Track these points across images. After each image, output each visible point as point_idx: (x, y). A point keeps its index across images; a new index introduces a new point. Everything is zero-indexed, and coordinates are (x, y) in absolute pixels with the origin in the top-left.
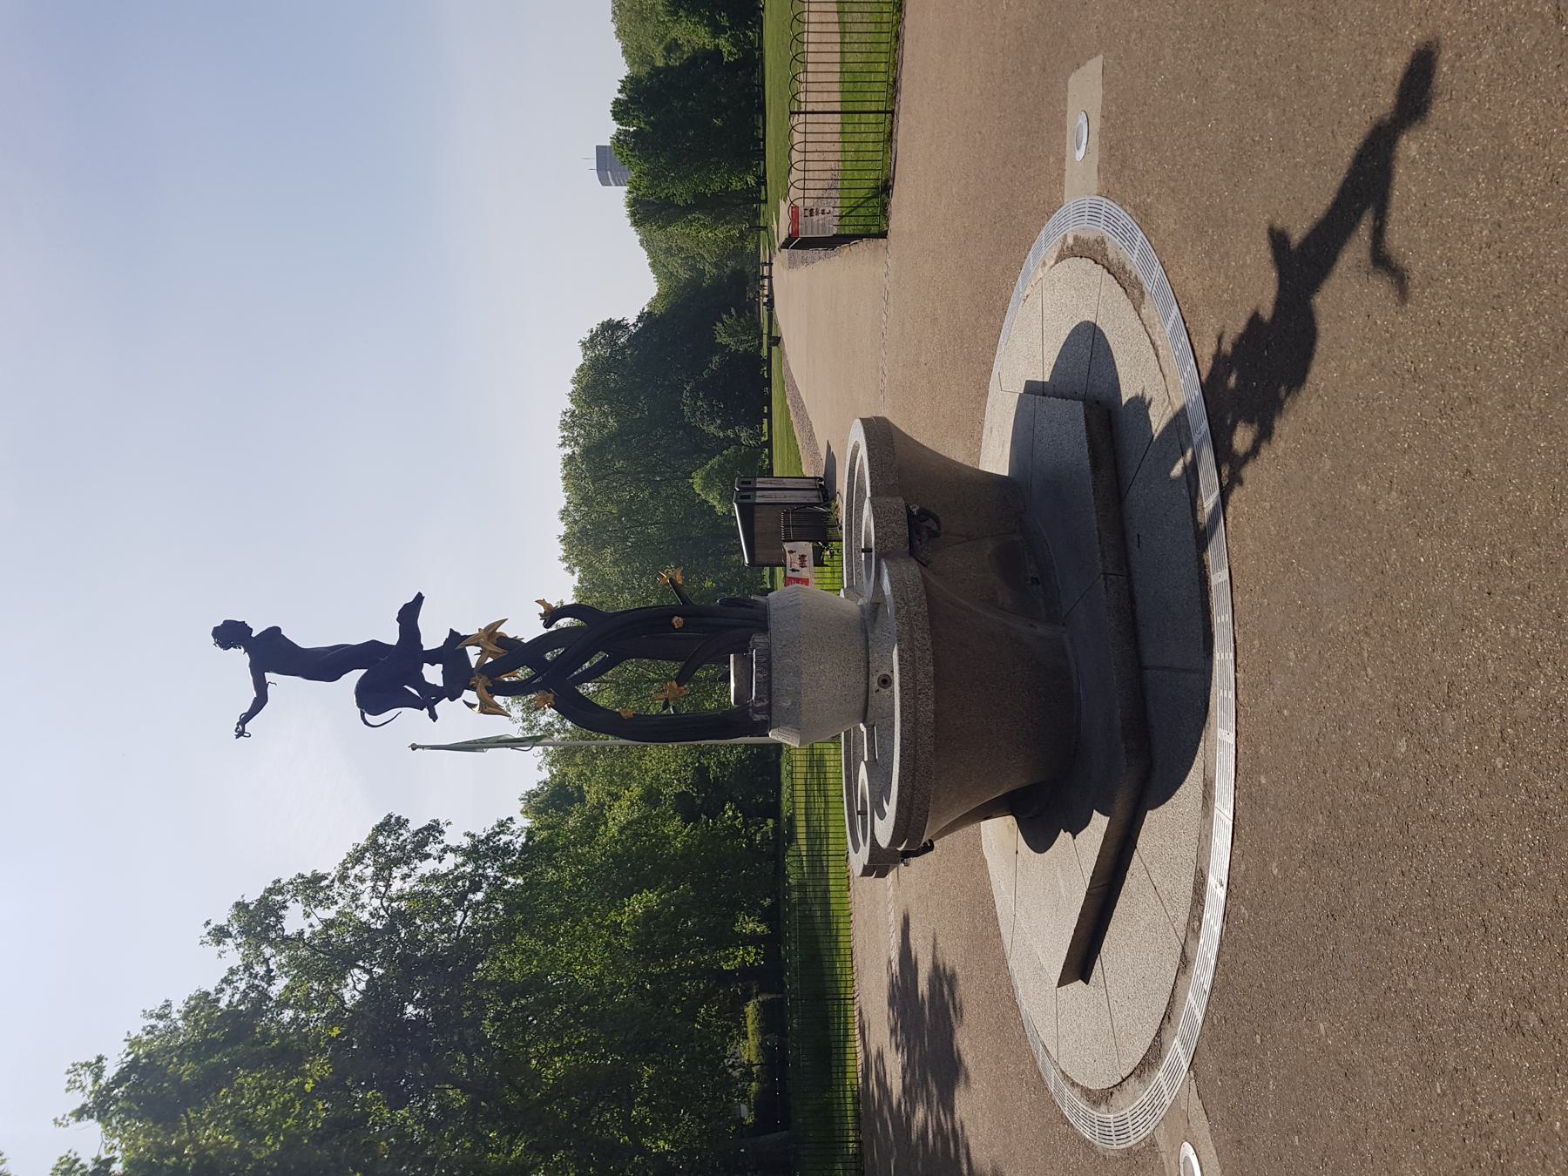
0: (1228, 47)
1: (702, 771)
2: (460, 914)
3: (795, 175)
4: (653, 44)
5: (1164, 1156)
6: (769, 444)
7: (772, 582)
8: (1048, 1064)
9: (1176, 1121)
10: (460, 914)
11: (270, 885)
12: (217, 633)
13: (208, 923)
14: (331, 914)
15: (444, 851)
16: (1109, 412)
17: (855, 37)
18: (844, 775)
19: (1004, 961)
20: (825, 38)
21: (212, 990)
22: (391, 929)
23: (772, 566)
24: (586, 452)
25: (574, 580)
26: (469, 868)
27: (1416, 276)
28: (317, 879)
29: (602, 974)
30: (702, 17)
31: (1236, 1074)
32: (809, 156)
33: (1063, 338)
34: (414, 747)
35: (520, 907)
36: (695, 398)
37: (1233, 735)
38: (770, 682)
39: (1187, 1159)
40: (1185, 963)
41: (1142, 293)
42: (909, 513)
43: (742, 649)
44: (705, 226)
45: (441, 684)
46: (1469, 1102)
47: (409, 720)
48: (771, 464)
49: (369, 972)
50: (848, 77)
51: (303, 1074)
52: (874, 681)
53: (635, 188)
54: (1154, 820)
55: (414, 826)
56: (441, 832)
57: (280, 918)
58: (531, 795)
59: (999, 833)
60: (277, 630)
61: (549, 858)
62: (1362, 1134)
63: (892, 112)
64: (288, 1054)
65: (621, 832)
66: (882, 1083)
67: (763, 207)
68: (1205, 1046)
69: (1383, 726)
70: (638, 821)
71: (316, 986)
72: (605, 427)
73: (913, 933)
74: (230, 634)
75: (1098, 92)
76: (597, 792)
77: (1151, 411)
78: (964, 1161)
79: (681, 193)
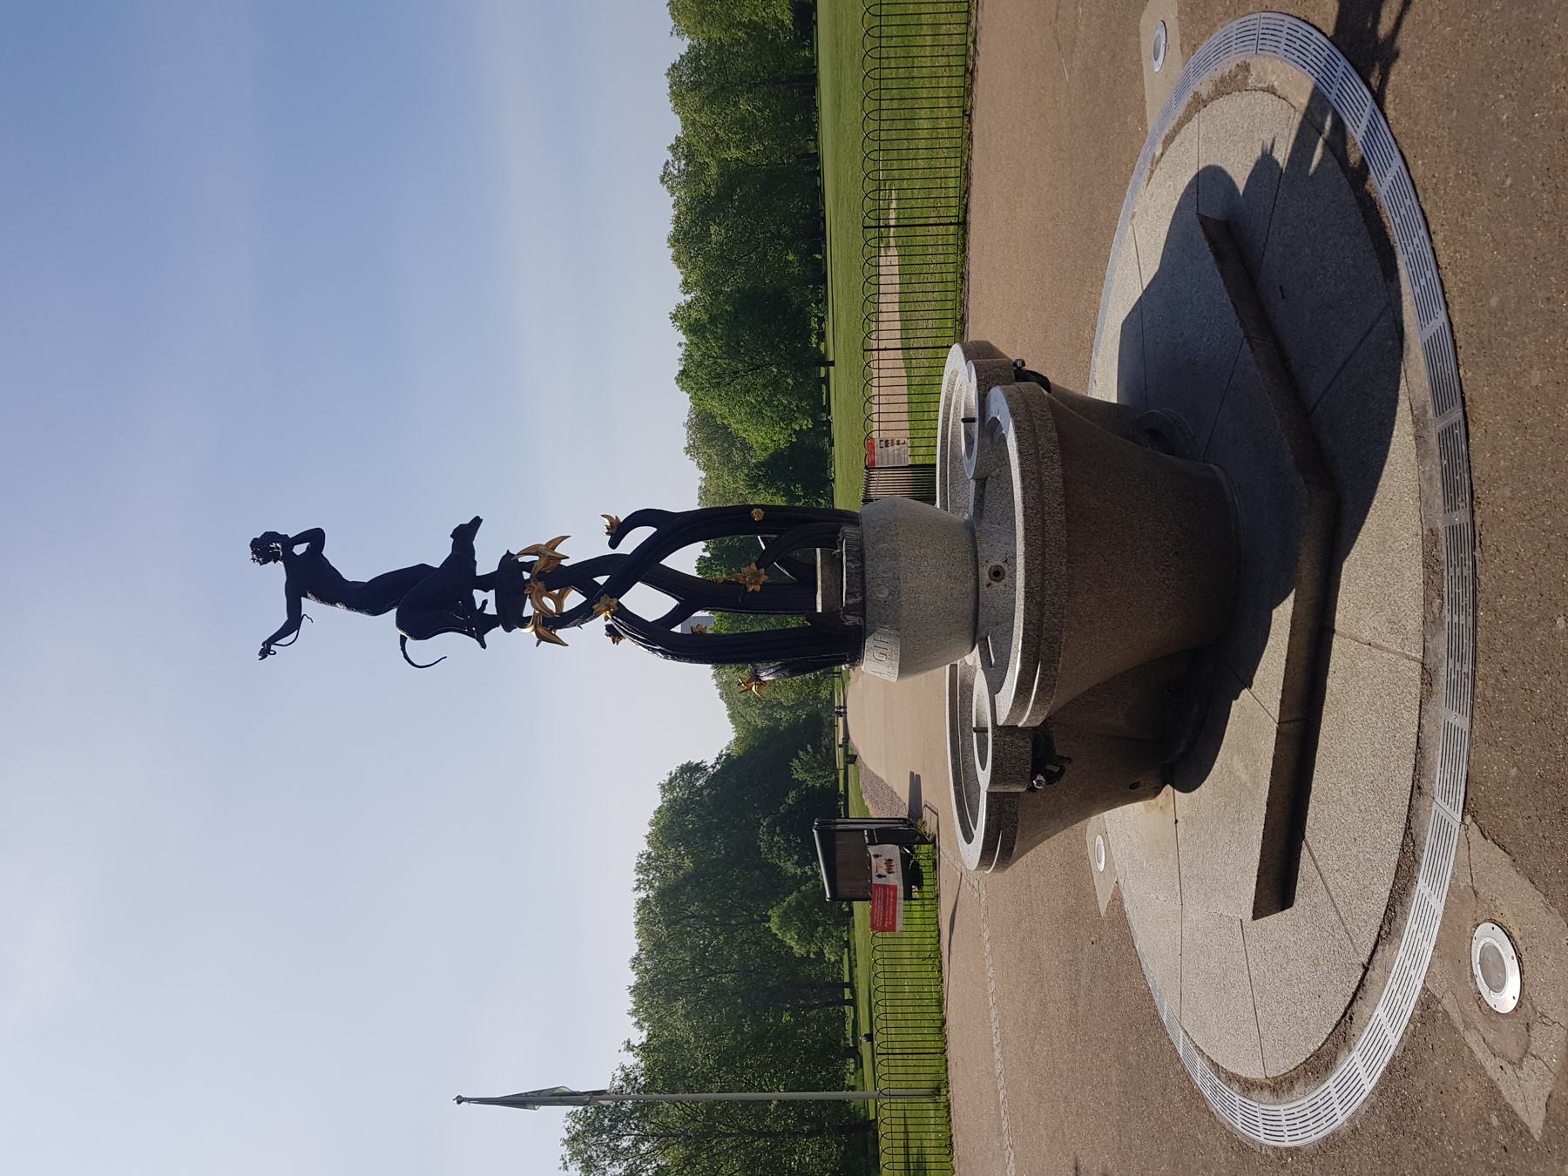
12: (255, 544)
24: (661, 895)
34: (460, 1100)
36: (772, 833)
38: (863, 573)
43: (830, 543)
54: (1354, 571)
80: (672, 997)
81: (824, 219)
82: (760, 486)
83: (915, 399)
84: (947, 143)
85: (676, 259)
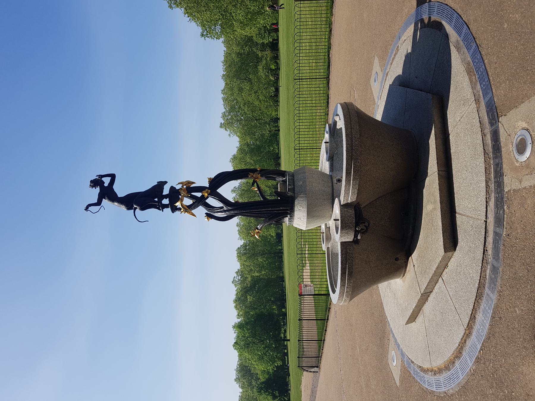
81: (285, 287)
82: (262, 392)
85: (236, 307)
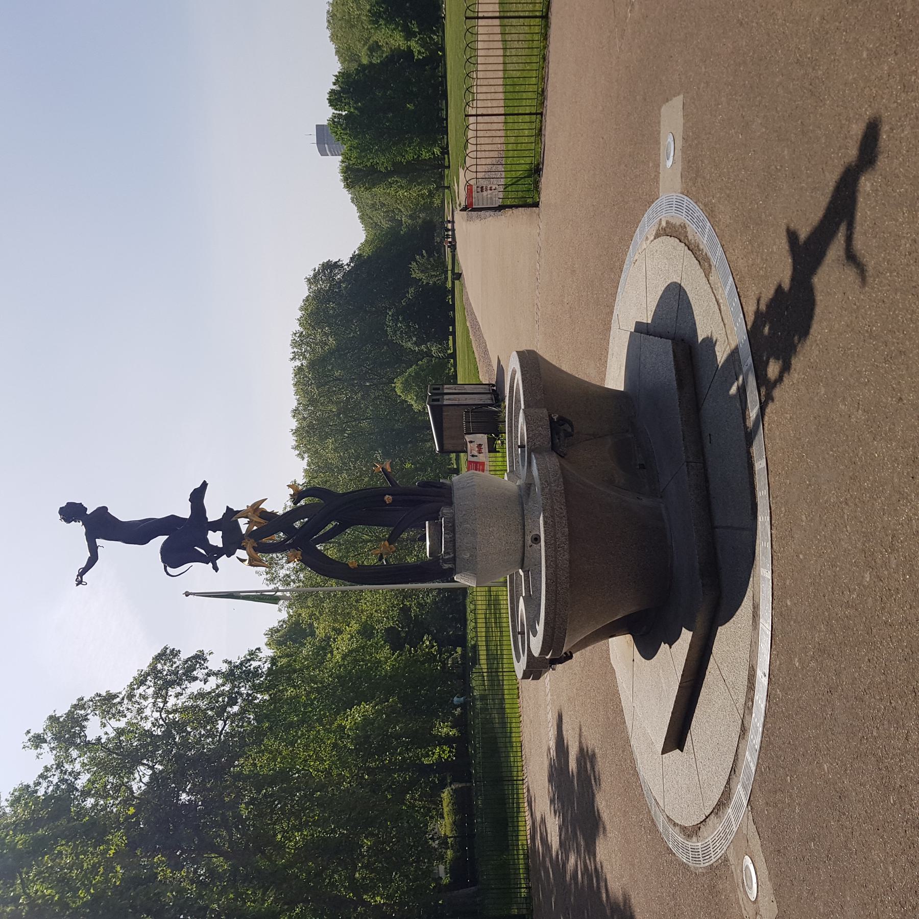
0: (760, 102)
1: (405, 610)
2: (221, 723)
3: (471, 148)
4: (359, 46)
5: (733, 867)
6: (454, 356)
7: (458, 464)
8: (658, 812)
9: (740, 842)
10: (221, 723)
11: (75, 702)
13: (28, 732)
14: (122, 724)
15: (208, 675)
16: (690, 347)
17: (514, 52)
18: (508, 604)
19: (627, 741)
20: (492, 45)
21: (32, 785)
22: (168, 735)
23: (458, 452)
24: (312, 365)
25: (304, 464)
26: (227, 688)
27: (870, 270)
28: (110, 697)
29: (330, 768)
30: (397, 25)
31: (776, 805)
32: (480, 134)
33: (660, 293)
35: (267, 717)
36: (396, 321)
37: (770, 572)
39: (747, 867)
40: (744, 731)
41: (710, 265)
42: (551, 419)
43: (434, 517)
44: (402, 187)
45: (221, 545)
46: (908, 807)
47: (197, 574)
48: (455, 371)
49: (152, 768)
50: (509, 82)
51: (107, 842)
52: (529, 539)
53: (346, 158)
55: (184, 656)
56: (205, 660)
57: (83, 728)
58: (273, 631)
59: (621, 647)
60: (105, 508)
61: (289, 679)
62: (850, 836)
63: (541, 114)
64: (95, 829)
65: (343, 658)
66: (544, 841)
67: (446, 171)
68: (757, 787)
69: (856, 564)
70: (356, 650)
71: (111, 779)
72: (326, 344)
73: (565, 727)
74: (72, 512)
75: (681, 121)
76: (324, 628)
77: (717, 348)
78: (603, 891)
79: (383, 162)
80: (323, 438)
83: (510, 96)
84: (526, 132)
